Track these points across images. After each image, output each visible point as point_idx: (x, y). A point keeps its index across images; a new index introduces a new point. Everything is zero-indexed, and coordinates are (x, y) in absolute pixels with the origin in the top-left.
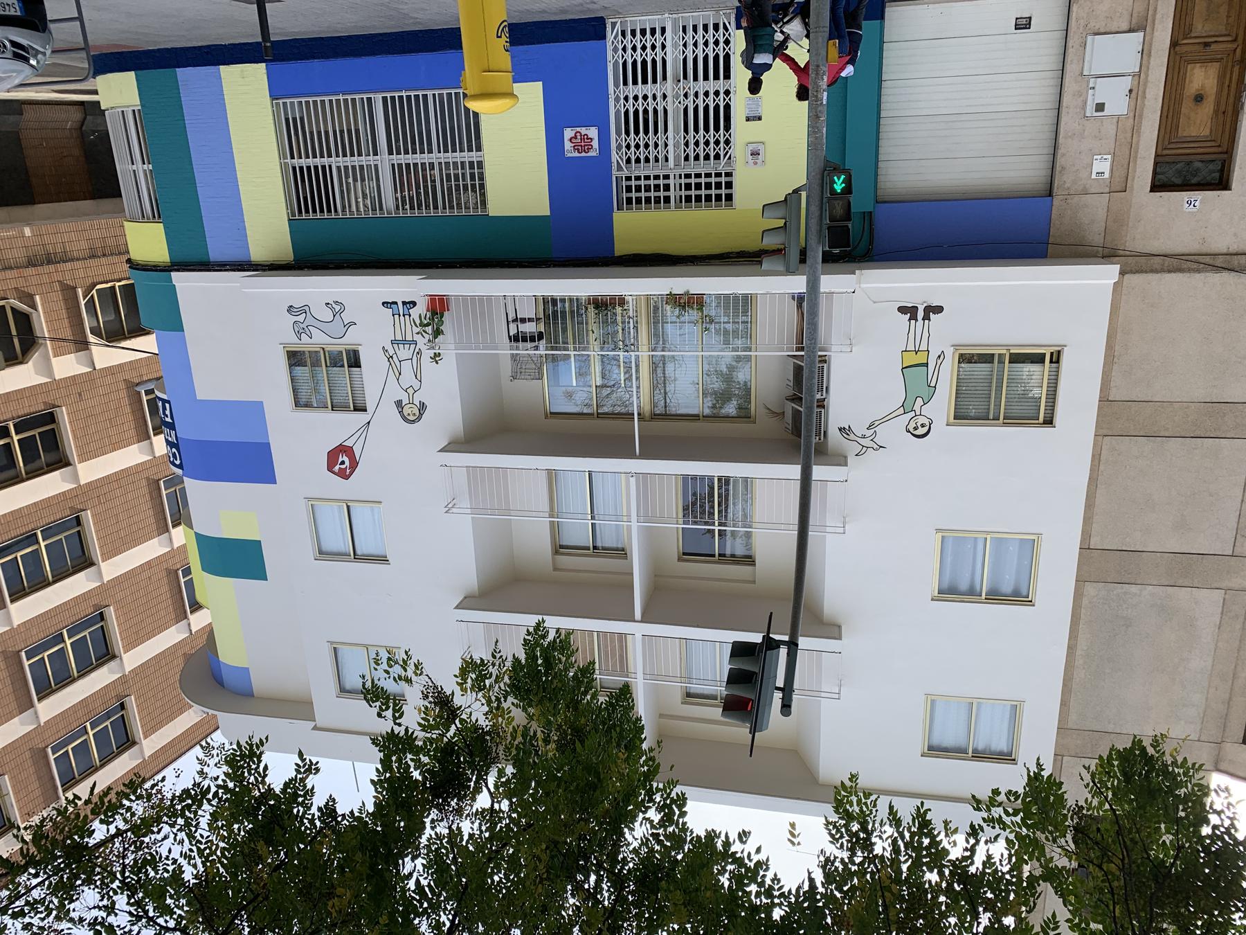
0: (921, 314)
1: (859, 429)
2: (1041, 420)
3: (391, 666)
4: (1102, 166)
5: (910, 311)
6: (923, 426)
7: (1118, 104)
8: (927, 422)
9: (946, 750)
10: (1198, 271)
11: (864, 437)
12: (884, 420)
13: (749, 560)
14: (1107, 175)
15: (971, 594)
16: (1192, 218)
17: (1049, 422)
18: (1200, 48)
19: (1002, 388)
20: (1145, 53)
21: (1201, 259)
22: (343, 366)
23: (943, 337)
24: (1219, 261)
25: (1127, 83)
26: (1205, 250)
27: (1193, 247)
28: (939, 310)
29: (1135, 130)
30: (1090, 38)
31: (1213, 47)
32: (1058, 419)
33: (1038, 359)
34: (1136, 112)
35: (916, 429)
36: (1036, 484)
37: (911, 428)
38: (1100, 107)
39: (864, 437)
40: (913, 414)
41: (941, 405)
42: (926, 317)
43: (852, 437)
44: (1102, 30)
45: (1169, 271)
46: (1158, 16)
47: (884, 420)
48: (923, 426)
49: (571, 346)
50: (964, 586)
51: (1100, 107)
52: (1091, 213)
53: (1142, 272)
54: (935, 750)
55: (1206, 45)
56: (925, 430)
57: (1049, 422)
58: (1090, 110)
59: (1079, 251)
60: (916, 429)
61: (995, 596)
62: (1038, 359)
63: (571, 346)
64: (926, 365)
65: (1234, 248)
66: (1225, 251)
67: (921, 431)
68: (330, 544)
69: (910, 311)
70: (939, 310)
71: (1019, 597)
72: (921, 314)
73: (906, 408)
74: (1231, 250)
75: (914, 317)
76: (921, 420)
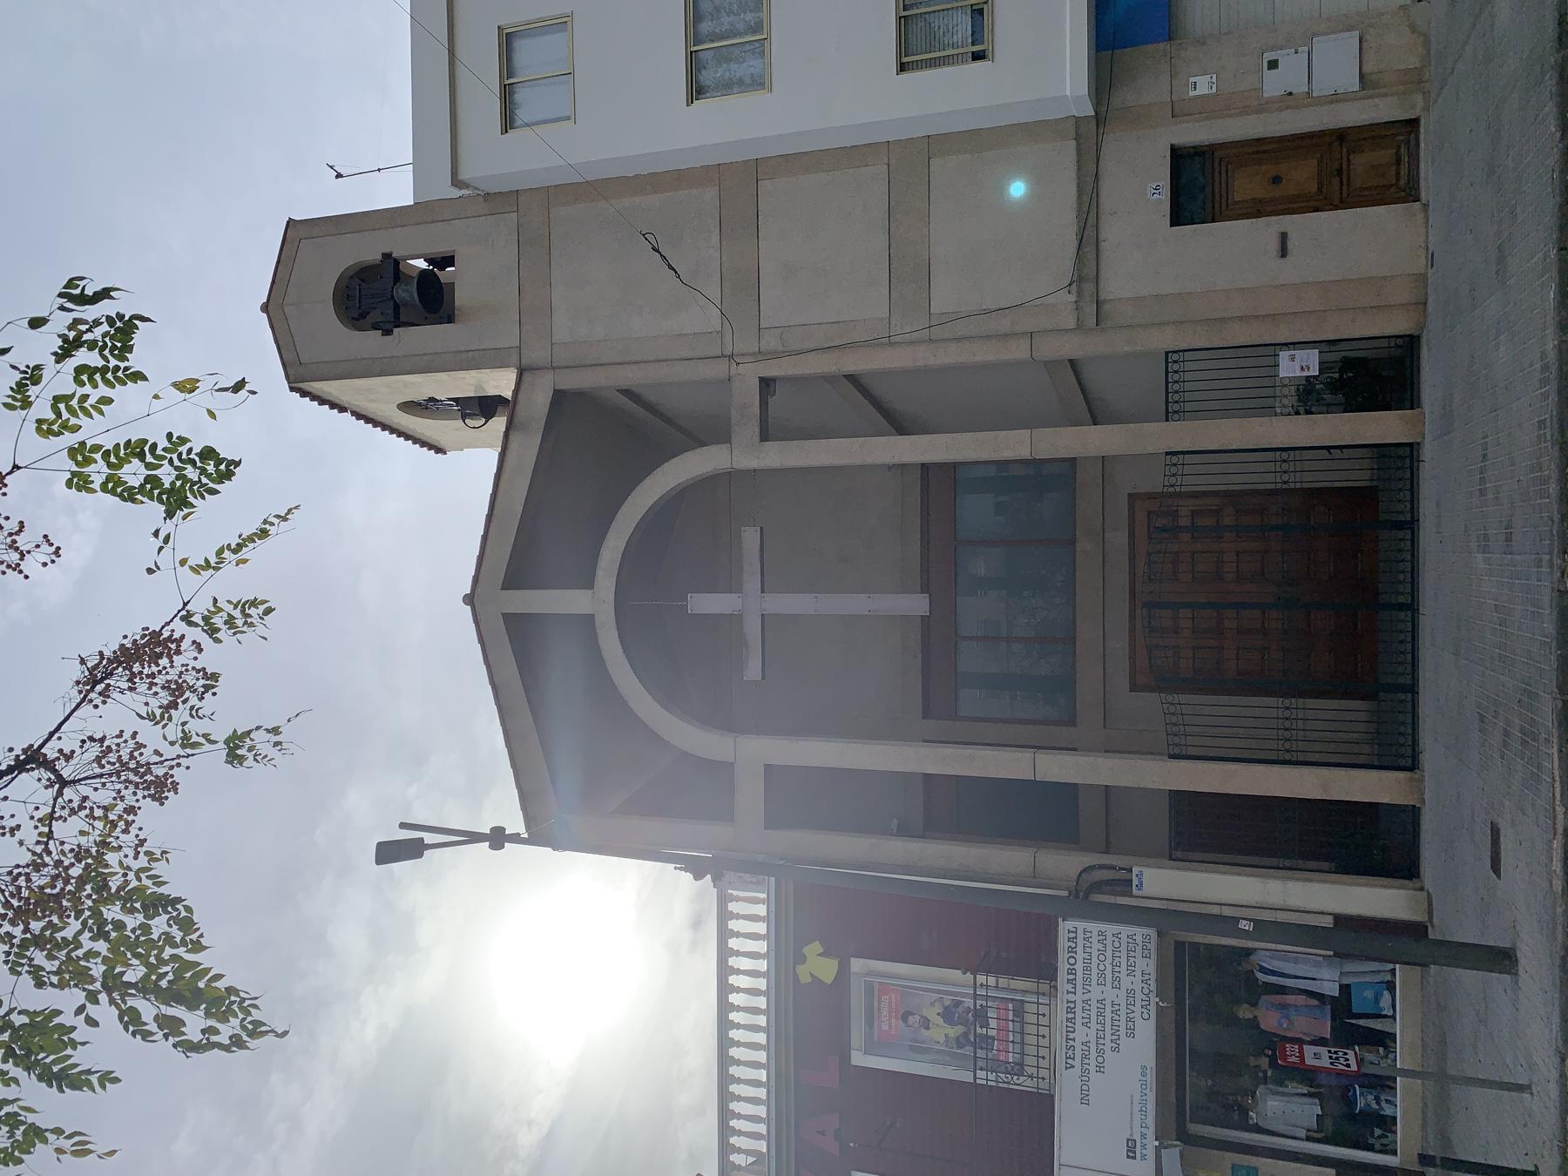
2: (905, 60)
3: (148, 479)
4: (1203, 85)
7: (1274, 85)
9: (509, 59)
14: (1192, 93)
16: (1139, 181)
17: (902, 68)
18: (1336, 165)
20: (1335, 98)
22: (973, 44)
24: (1090, 232)
25: (1300, 87)
27: (1107, 202)
29: (1246, 111)
30: (1356, 33)
32: (905, 76)
33: (977, 34)
34: (1265, 107)
38: (1273, 65)
44: (1365, 45)
50: (706, 27)
51: (1273, 65)
52: (1148, 88)
54: (507, 41)
55: (1340, 172)
57: (902, 68)
58: (1268, 56)
59: (1103, 81)
61: (694, 63)
62: (977, 34)
66: (1102, 237)
68: (525, 51)
74: (1102, 244)
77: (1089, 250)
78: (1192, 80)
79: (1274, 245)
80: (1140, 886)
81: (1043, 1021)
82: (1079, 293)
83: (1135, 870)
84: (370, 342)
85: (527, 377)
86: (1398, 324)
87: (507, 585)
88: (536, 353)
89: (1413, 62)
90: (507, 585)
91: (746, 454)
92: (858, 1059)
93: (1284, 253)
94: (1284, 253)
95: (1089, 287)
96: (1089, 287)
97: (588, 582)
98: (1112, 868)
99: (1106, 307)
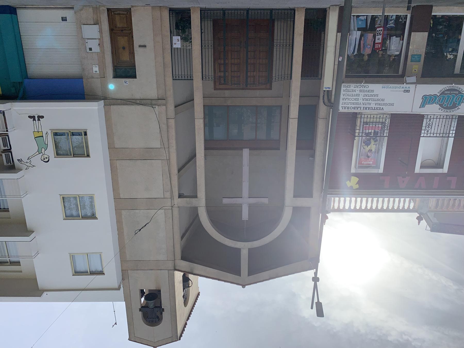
0: (36, 119)
1: (25, 160)
2: (86, 155)
4: (96, 69)
5: (33, 117)
6: (46, 158)
7: (96, 49)
8: (47, 157)
10: (132, 105)
11: (27, 162)
12: (33, 156)
13: (10, 218)
14: (98, 72)
15: (77, 217)
19: (71, 145)
20: (101, 31)
21: (132, 101)
23: (46, 126)
25: (97, 42)
26: (133, 98)
28: (42, 117)
29: (104, 57)
30: (82, 26)
31: (124, 31)
32: (91, 155)
33: (80, 134)
34: (103, 51)
35: (44, 159)
36: (90, 176)
37: (43, 158)
38: (91, 49)
39: (27, 162)
40: (42, 154)
41: (51, 151)
42: (39, 120)
43: (23, 162)
44: (85, 23)
45: (124, 105)
46: (102, 20)
47: (33, 156)
48: (46, 158)
49: (238, 201)
53: (115, 105)
54: (77, 273)
55: (122, 30)
56: (48, 159)
57: (88, 156)
58: (88, 50)
59: (93, 98)
60: (44, 159)
62: (80, 134)
63: (238, 201)
64: (43, 136)
65: (142, 98)
66: (139, 98)
67: (46, 160)
69: (33, 117)
70: (42, 117)
71: (93, 217)
72: (36, 119)
73: (39, 152)
75: (34, 120)
76: (45, 156)
77: (143, 102)
78: (94, 72)
79: (142, 49)
80: (329, 88)
81: (369, 117)
82: (156, 105)
83: (324, 89)
84: (166, 315)
85: (177, 268)
86: (166, 14)
87: (249, 274)
88: (170, 265)
89: (91, 10)
90: (249, 274)
91: (201, 202)
92: (381, 170)
93: (145, 46)
94: (145, 46)
95: (154, 102)
96: (154, 102)
97: (238, 251)
98: (324, 96)
99: (160, 97)
